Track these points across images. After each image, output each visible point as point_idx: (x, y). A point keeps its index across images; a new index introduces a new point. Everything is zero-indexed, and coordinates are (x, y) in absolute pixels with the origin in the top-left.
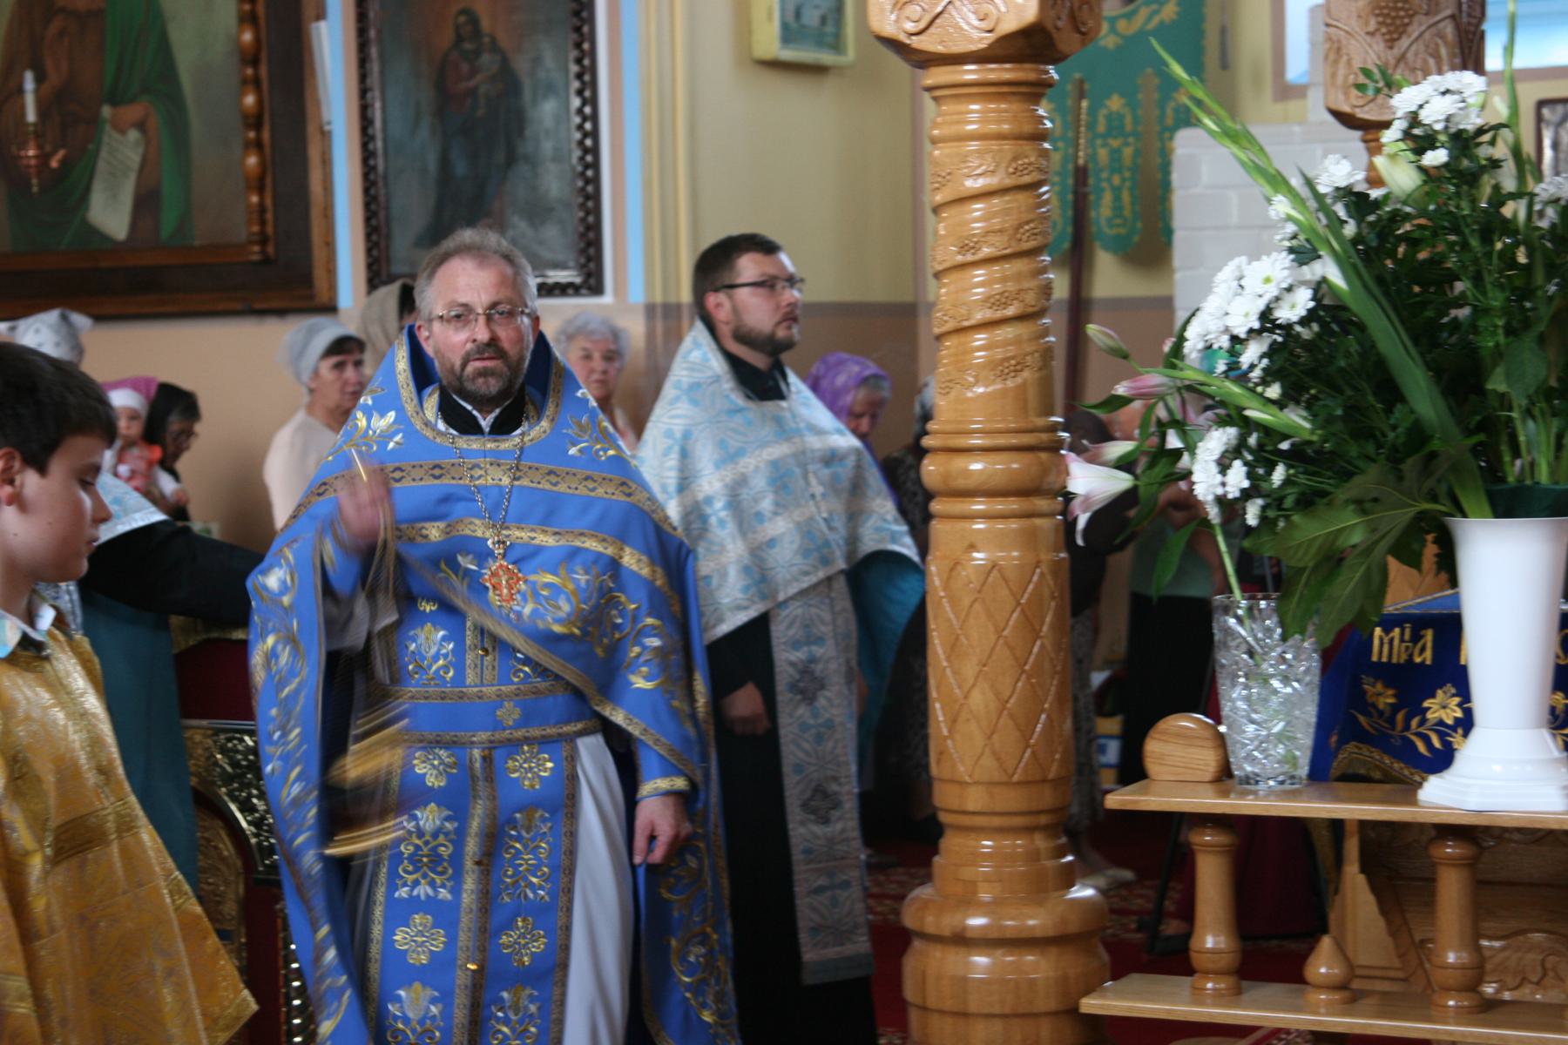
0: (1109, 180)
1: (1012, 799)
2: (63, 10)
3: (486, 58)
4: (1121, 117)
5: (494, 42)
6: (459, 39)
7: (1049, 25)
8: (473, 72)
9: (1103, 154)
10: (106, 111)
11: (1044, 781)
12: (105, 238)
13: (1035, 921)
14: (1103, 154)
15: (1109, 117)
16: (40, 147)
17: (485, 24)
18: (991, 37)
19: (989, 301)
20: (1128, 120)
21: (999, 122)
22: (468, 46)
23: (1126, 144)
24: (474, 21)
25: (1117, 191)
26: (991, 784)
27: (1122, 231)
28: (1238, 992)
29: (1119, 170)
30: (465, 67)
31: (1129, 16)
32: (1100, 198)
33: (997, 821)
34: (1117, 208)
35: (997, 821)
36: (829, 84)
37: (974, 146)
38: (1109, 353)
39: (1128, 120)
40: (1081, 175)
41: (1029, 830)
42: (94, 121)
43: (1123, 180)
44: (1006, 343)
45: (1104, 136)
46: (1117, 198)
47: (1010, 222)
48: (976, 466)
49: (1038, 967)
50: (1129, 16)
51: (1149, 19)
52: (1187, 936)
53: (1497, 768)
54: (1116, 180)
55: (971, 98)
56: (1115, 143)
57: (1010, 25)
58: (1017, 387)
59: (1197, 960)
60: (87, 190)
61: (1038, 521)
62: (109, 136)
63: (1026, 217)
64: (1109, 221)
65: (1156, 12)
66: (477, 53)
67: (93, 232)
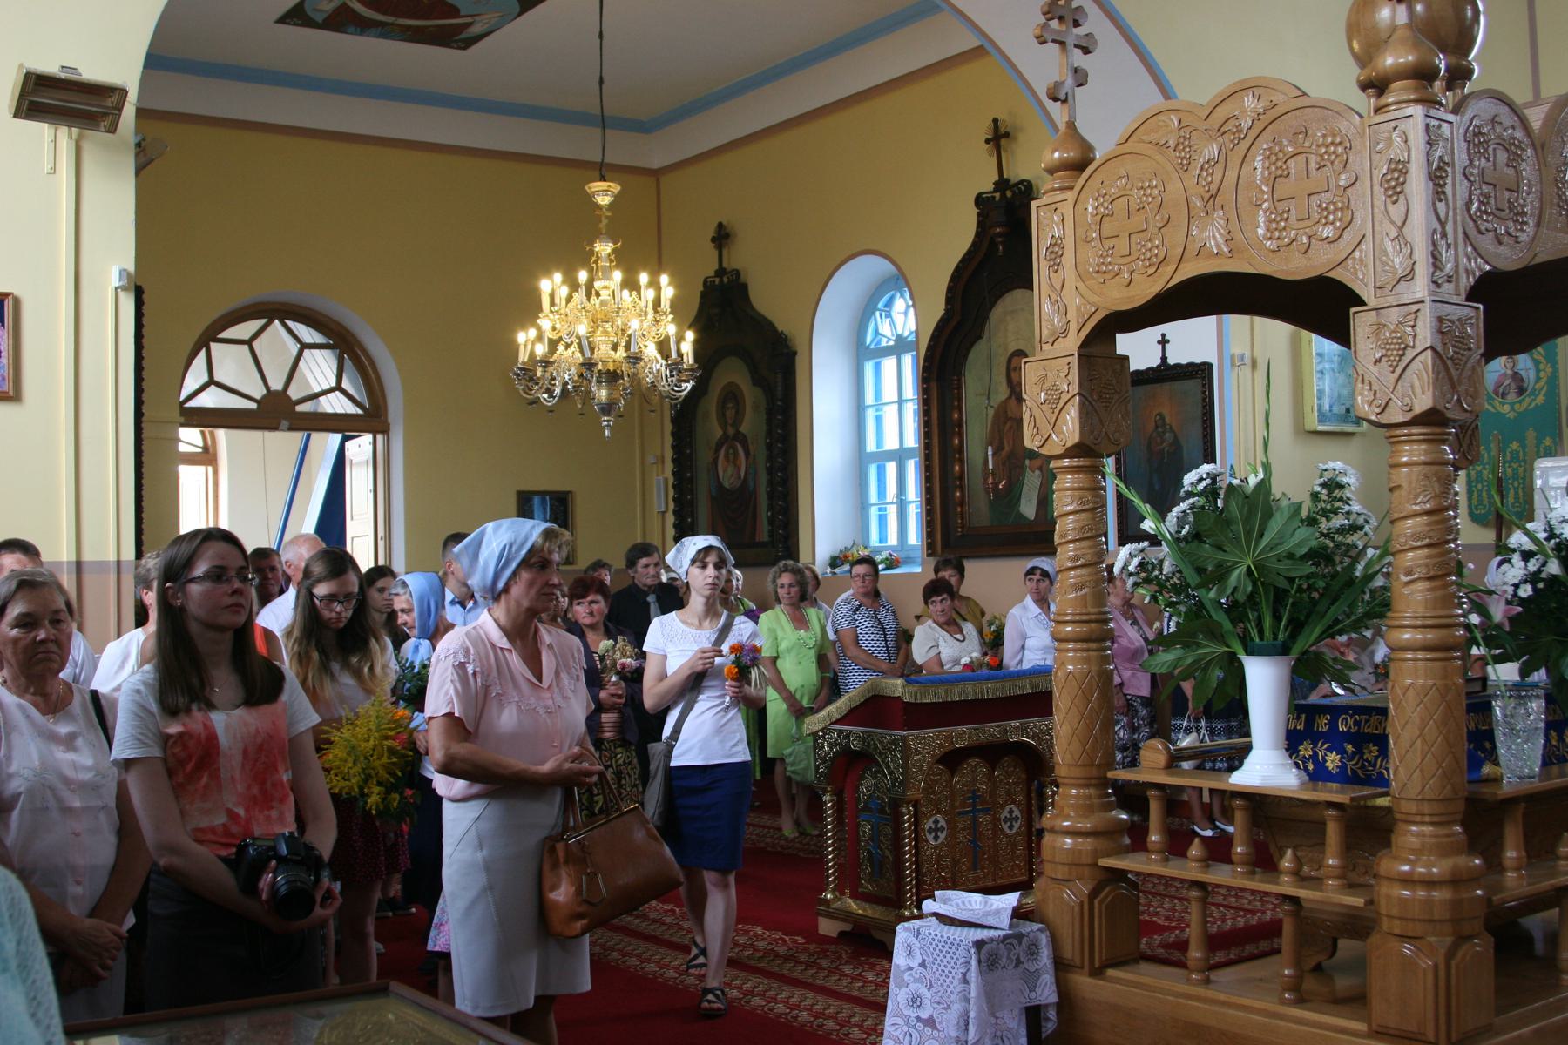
0: (1476, 486)
1: (1077, 772)
2: (1011, 418)
3: (1167, 435)
4: (1518, 453)
5: (1171, 428)
6: (1157, 427)
7: (1440, 407)
8: (1163, 442)
9: (1509, 471)
10: (1027, 462)
11: (1093, 765)
12: (1026, 518)
13: (1087, 825)
14: (1509, 471)
15: (1511, 453)
16: (994, 479)
17: (1168, 420)
18: (1064, 448)
19: (1074, 559)
20: (1521, 454)
21: (1419, 455)
22: (1160, 430)
23: (1485, 469)
24: (1163, 418)
25: (1516, 489)
26: (1069, 765)
27: (1519, 510)
28: (1253, 873)
29: (1517, 480)
30: (1159, 440)
31: (1520, 402)
32: (1508, 493)
33: (1072, 781)
34: (1516, 498)
35: (1072, 781)
36: (1355, 441)
37: (1069, 493)
38: (136, 601)
39: (1521, 454)
40: (1500, 481)
41: (1087, 786)
42: (1022, 467)
43: (1483, 486)
44: (1082, 576)
45: (1510, 462)
46: (1516, 493)
47: (1078, 525)
48: (1069, 629)
49: (1087, 844)
50: (1520, 402)
51: (1530, 404)
52: (1323, 858)
53: (1258, 767)
54: (1516, 484)
55: (1069, 473)
56: (1515, 466)
57: (1070, 444)
58: (1082, 595)
59: (1150, 846)
60: (1019, 499)
61: (1091, 653)
62: (1028, 473)
63: (1085, 523)
64: (1513, 505)
65: (1534, 400)
66: (1164, 433)
67: (1021, 516)
